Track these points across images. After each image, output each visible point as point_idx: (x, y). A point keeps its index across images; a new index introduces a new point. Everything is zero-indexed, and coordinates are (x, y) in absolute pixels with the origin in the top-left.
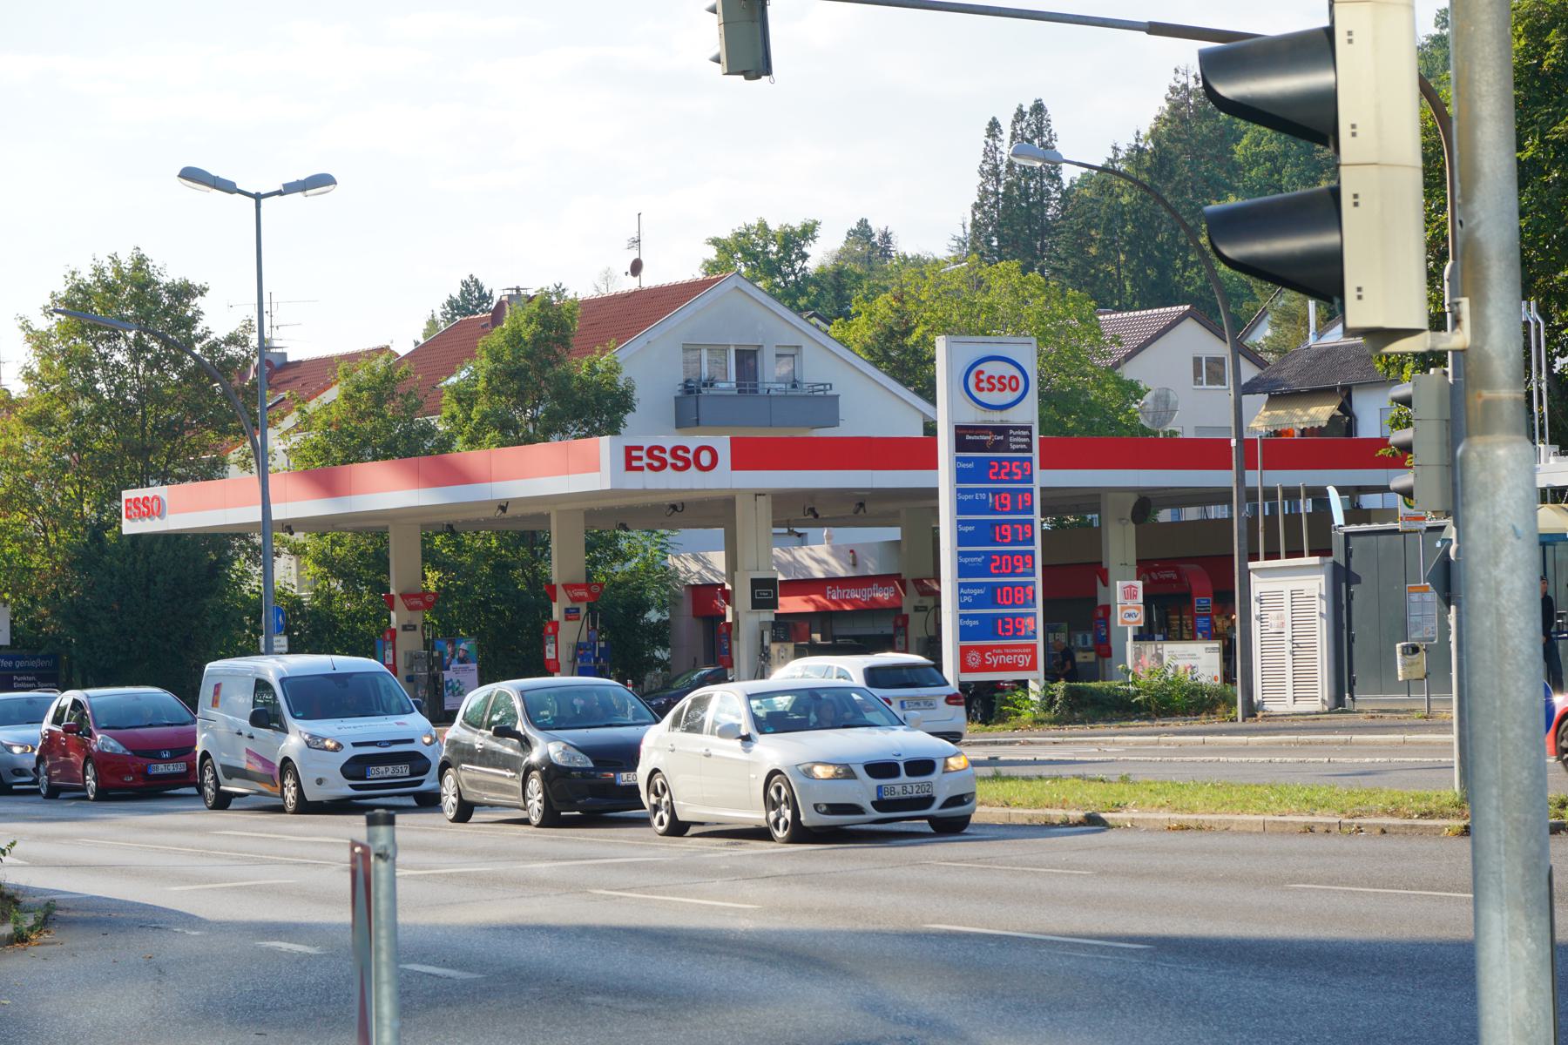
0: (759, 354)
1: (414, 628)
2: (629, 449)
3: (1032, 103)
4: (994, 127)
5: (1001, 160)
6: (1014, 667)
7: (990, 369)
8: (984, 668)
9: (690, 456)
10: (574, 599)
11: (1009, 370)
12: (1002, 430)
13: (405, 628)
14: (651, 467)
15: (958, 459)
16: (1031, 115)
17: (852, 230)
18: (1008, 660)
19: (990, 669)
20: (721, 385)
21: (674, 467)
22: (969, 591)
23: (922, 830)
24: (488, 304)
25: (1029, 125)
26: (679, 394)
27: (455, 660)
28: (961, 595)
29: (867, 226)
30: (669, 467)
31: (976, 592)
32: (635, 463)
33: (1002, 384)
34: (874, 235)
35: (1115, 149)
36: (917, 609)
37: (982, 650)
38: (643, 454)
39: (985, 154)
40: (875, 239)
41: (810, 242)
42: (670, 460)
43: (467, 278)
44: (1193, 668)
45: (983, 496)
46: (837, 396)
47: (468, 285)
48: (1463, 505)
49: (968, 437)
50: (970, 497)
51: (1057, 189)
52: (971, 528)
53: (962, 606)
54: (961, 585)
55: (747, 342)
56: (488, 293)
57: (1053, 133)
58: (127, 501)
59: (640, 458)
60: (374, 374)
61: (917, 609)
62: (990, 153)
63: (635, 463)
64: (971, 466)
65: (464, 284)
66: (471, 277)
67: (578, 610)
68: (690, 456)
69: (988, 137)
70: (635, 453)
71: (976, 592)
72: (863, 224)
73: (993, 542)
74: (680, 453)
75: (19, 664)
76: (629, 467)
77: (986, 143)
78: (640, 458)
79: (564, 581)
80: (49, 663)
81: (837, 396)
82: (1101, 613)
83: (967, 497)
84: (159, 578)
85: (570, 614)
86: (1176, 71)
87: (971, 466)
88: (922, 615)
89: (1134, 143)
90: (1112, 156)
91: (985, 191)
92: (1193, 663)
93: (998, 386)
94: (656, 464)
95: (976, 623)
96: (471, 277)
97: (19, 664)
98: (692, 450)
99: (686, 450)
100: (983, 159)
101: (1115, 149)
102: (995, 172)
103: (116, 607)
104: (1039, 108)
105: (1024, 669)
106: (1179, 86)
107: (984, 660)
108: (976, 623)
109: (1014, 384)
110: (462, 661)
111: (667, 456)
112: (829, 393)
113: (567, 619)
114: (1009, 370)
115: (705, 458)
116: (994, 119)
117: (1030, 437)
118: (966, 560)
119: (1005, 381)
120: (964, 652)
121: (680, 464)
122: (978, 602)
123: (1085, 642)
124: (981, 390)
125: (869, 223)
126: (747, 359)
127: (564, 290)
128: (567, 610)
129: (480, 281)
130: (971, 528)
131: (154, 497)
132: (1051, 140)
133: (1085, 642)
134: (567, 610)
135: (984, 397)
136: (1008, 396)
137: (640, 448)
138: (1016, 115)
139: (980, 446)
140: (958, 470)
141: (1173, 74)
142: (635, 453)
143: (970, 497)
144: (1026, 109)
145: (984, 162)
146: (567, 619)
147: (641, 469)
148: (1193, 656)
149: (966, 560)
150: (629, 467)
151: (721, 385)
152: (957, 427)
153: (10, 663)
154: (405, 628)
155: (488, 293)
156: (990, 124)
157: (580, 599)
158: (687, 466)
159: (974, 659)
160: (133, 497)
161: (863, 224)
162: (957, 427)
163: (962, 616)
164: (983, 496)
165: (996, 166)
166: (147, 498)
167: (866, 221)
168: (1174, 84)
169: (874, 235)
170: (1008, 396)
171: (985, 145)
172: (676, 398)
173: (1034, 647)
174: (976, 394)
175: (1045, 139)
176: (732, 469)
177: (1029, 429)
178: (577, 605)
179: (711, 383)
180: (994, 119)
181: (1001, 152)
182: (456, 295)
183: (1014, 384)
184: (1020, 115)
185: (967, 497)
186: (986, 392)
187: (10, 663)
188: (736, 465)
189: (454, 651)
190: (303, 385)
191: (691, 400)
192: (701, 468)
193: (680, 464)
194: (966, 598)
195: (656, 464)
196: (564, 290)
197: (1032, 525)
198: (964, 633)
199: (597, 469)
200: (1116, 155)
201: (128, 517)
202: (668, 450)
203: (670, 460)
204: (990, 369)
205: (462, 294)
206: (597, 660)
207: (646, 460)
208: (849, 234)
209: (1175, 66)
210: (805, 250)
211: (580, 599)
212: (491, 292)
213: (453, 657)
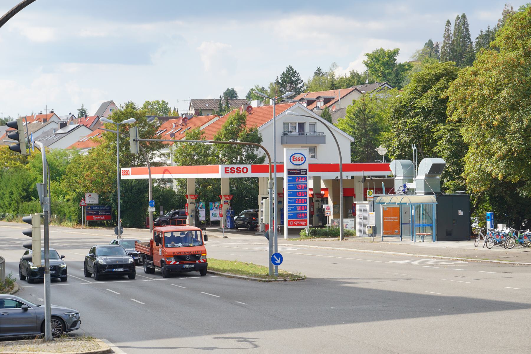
0: (305, 124)
1: (193, 203)
2: (226, 168)
3: (462, 14)
4: (448, 23)
5: (450, 33)
6: (301, 225)
7: (296, 156)
8: (294, 225)
9: (241, 170)
10: (226, 199)
11: (301, 156)
12: (300, 170)
13: (191, 203)
14: (231, 172)
15: (288, 177)
16: (461, 18)
17: (426, 43)
18: (300, 223)
19: (296, 225)
20: (294, 133)
21: (237, 172)
22: (290, 207)
23: (197, 274)
24: (295, 74)
25: (460, 21)
26: (282, 135)
27: (215, 208)
28: (288, 208)
29: (431, 42)
30: (236, 172)
31: (292, 208)
32: (227, 172)
33: (299, 159)
34: (433, 45)
35: (482, 32)
36: (316, 201)
37: (294, 221)
38: (229, 169)
39: (445, 31)
40: (434, 46)
41: (397, 55)
42: (236, 171)
43: (288, 66)
44: (347, 225)
45: (294, 185)
46: (325, 136)
47: (289, 69)
48: (124, 262)
49: (291, 172)
50: (291, 186)
51: (469, 42)
52: (291, 193)
53: (289, 211)
54: (288, 206)
55: (301, 121)
56: (295, 71)
57: (468, 24)
58: (122, 171)
59: (228, 170)
60: (195, 133)
61: (316, 201)
62: (447, 31)
63: (227, 172)
64: (291, 178)
65: (287, 68)
66: (290, 66)
67: (227, 202)
68: (241, 170)
69: (446, 26)
70: (227, 169)
71: (292, 208)
72: (430, 41)
73: (297, 196)
74: (239, 169)
75: (101, 208)
76: (226, 172)
77: (446, 27)
78: (228, 170)
79: (224, 194)
80: (108, 208)
81: (325, 136)
82: (354, 205)
83: (290, 186)
84: (134, 188)
85: (225, 202)
86: (506, 5)
87: (291, 178)
88: (318, 202)
89: (488, 30)
90: (480, 34)
91: (446, 43)
92: (347, 224)
93: (298, 160)
94: (232, 172)
95: (292, 215)
96: (290, 66)
97: (101, 208)
98: (242, 168)
99: (240, 168)
100: (444, 32)
101: (482, 32)
102: (449, 37)
103: (123, 195)
104: (464, 16)
105: (304, 225)
106: (506, 10)
107: (294, 223)
108: (292, 215)
109: (302, 160)
110: (216, 208)
111: (235, 170)
112: (323, 135)
113: (225, 204)
114: (301, 156)
115: (245, 170)
116: (448, 20)
117: (306, 171)
118: (290, 200)
119: (300, 159)
120: (289, 221)
121: (238, 171)
122: (292, 210)
123: (351, 212)
124: (294, 161)
125: (432, 41)
126: (302, 126)
127: (321, 69)
128: (225, 202)
129: (292, 67)
130: (291, 193)
131: (128, 170)
132: (467, 26)
133: (351, 212)
134: (225, 202)
135: (295, 162)
136: (301, 162)
137: (229, 168)
138: (457, 18)
139: (294, 174)
140: (288, 179)
141: (504, 6)
142: (227, 169)
143: (291, 186)
144: (460, 16)
145: (445, 33)
146: (225, 204)
147: (229, 173)
148: (347, 222)
149: (290, 200)
150: (226, 172)
151: (294, 133)
152: (288, 170)
153: (98, 208)
154: (191, 203)
155: (295, 71)
156: (447, 22)
157: (228, 199)
158: (240, 172)
159: (291, 223)
160: (123, 170)
161: (430, 41)
162: (288, 170)
163: (288, 213)
164: (294, 185)
165: (449, 35)
166: (126, 170)
167: (431, 40)
168: (505, 9)
169: (433, 45)
170: (301, 162)
171: (445, 28)
172: (281, 136)
173: (306, 220)
174: (303, 157)
175: (466, 26)
176: (252, 172)
177: (306, 170)
178: (227, 200)
179: (291, 132)
180: (448, 20)
181: (450, 31)
182: (285, 72)
183: (302, 160)
184: (458, 18)
185: (290, 186)
186: (295, 161)
187: (98, 208)
188: (252, 172)
189: (215, 205)
190: (194, 125)
191: (285, 137)
192: (244, 173)
193: (238, 171)
194: (290, 209)
195: (232, 172)
196: (321, 69)
197: (306, 192)
198: (289, 217)
199: (218, 173)
200: (482, 34)
201: (122, 175)
202: (236, 168)
203: (236, 171)
204: (296, 156)
205: (287, 72)
206: (231, 214)
207: (230, 171)
208: (425, 44)
209: (505, 3)
210: (395, 57)
211: (228, 199)
212: (296, 71)
213: (214, 207)
